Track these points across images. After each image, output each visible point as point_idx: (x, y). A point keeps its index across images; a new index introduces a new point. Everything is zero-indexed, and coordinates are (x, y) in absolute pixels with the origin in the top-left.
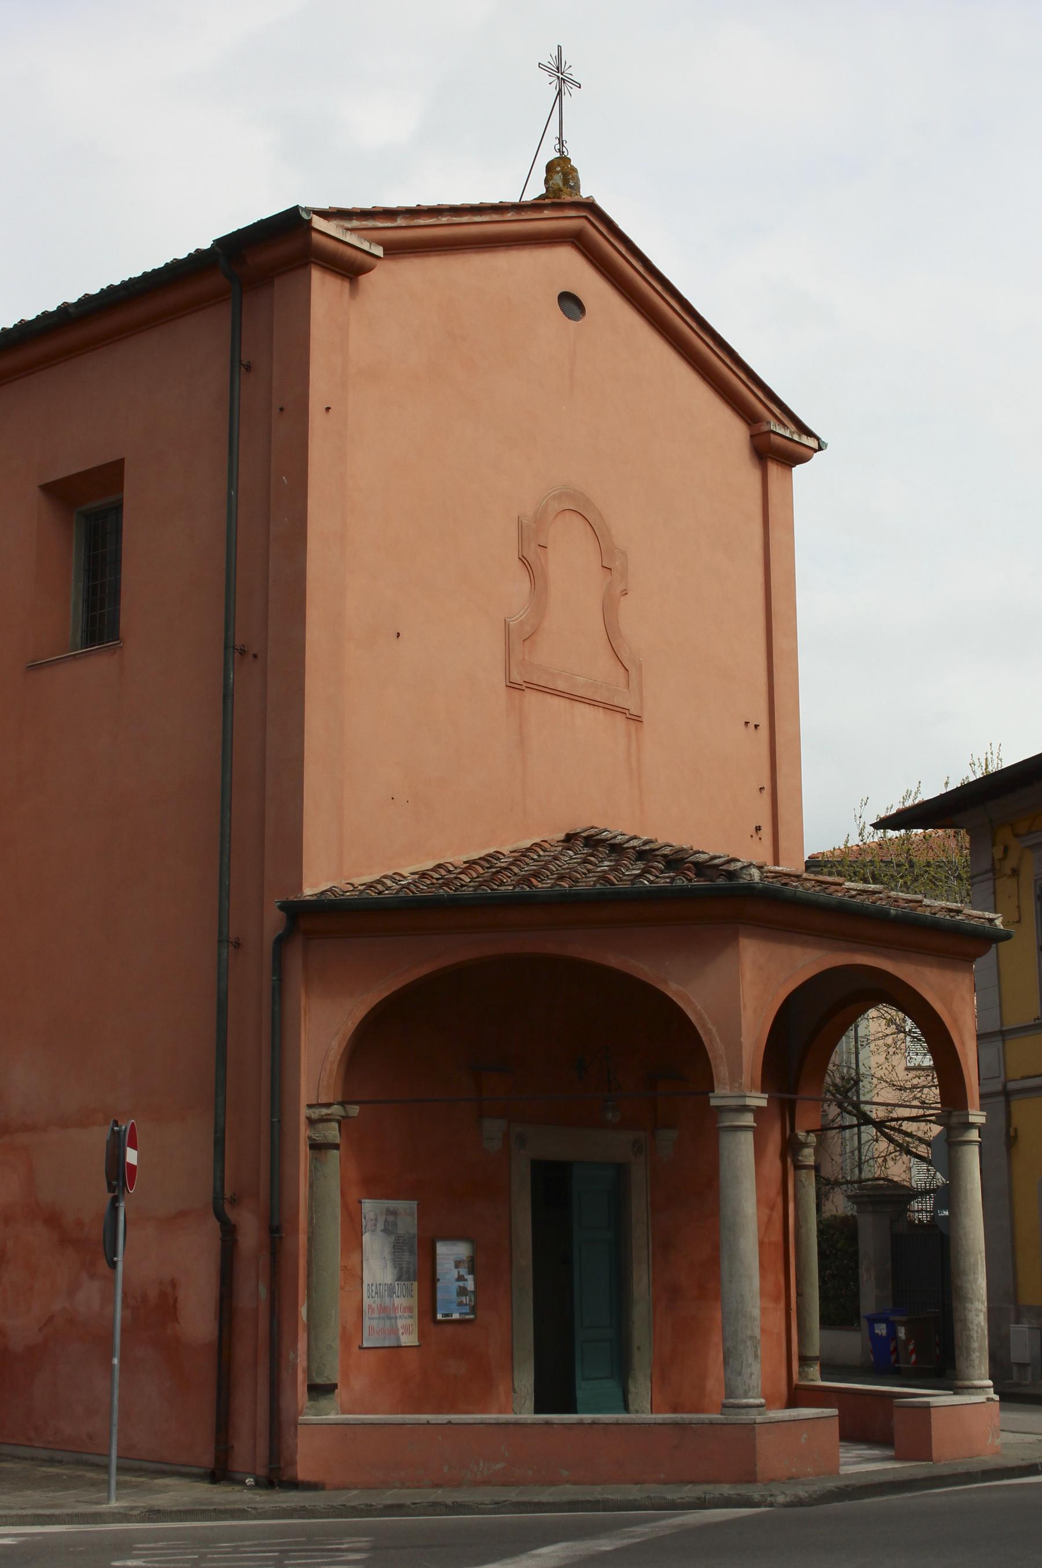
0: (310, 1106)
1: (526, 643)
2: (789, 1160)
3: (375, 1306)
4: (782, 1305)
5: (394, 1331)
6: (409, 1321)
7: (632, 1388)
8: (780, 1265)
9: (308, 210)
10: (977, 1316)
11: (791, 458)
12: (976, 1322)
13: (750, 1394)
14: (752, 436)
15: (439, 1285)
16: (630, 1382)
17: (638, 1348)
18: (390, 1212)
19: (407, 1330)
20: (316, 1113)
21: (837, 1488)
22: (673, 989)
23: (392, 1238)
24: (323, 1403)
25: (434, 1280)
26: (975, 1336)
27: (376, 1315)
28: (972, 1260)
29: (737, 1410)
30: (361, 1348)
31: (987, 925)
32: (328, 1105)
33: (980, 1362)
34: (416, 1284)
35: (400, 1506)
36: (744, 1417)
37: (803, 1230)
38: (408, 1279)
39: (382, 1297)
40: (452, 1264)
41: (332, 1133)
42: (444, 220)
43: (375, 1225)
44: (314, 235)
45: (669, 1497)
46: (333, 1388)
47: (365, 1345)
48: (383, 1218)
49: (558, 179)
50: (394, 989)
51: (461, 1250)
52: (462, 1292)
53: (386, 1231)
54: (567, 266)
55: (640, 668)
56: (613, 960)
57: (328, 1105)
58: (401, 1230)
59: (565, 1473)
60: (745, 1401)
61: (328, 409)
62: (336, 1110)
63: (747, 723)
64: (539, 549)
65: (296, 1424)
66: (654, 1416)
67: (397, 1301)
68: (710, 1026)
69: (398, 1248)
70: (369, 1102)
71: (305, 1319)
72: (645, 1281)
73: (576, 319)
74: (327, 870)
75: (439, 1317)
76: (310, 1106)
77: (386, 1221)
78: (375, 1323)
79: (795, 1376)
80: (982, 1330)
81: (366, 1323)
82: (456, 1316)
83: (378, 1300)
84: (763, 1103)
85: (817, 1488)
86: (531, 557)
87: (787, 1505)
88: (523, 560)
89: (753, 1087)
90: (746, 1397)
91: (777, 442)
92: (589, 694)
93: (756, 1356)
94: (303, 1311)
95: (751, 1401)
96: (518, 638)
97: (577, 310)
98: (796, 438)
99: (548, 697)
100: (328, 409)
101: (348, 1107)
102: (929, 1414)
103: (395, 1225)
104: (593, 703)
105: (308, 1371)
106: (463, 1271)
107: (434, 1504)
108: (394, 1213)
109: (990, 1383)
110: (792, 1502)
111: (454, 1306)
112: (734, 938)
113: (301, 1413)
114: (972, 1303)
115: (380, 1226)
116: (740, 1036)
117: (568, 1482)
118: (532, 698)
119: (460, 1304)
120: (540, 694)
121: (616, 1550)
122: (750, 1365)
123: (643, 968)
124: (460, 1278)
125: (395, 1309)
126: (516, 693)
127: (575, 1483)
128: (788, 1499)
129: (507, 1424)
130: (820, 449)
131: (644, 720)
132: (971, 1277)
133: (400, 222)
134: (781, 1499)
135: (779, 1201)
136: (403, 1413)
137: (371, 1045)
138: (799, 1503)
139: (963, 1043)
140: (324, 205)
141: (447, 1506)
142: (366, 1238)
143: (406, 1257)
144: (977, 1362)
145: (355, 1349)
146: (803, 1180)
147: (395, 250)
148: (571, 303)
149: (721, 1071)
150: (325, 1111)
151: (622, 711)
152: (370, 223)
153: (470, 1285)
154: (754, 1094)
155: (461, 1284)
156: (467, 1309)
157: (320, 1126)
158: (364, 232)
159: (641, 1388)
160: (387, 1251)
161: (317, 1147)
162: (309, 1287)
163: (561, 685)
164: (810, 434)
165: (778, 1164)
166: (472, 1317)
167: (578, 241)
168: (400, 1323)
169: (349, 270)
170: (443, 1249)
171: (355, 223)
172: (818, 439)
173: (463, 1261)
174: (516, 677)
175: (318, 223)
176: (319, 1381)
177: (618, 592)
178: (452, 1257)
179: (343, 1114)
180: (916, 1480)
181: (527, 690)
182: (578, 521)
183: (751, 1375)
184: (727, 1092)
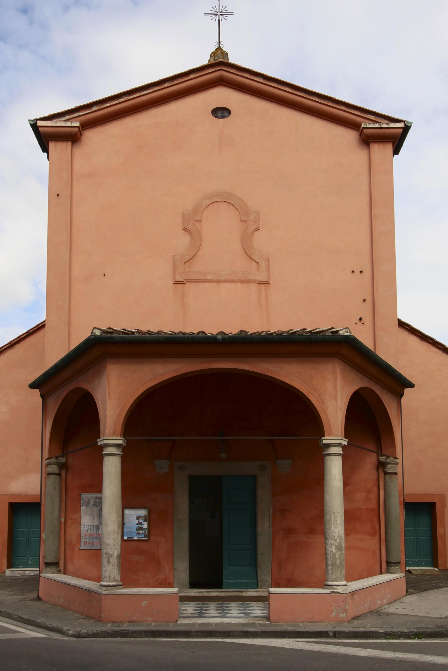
1: (187, 264)
2: (380, 471)
4: (377, 537)
7: (259, 571)
8: (376, 519)
10: (331, 547)
12: (330, 550)
13: (105, 580)
15: (125, 526)
16: (258, 568)
21: (113, 631)
26: (329, 558)
28: (328, 517)
30: (79, 549)
33: (332, 572)
37: (387, 503)
40: (135, 518)
44: (40, 129)
47: (81, 548)
51: (143, 512)
52: (141, 529)
54: (220, 96)
55: (268, 260)
64: (196, 223)
73: (225, 117)
77: (95, 501)
78: (87, 540)
81: (83, 540)
82: (136, 538)
86: (190, 227)
88: (185, 229)
89: (114, 434)
92: (230, 278)
97: (225, 113)
98: (384, 126)
99: (226, 283)
110: (74, 634)
111: (135, 534)
114: (328, 540)
119: (139, 534)
120: (197, 283)
124: (139, 523)
131: (271, 283)
134: (71, 632)
135: (375, 489)
140: (46, 114)
142: (83, 508)
144: (330, 572)
146: (387, 479)
148: (221, 112)
151: (254, 281)
152: (76, 115)
153: (145, 525)
154: (114, 438)
155: (140, 526)
163: (209, 277)
165: (375, 472)
166: (146, 539)
171: (67, 117)
172: (404, 121)
173: (142, 517)
174: (179, 279)
177: (252, 230)
178: (136, 515)
180: (191, 632)
181: (186, 283)
183: (105, 571)
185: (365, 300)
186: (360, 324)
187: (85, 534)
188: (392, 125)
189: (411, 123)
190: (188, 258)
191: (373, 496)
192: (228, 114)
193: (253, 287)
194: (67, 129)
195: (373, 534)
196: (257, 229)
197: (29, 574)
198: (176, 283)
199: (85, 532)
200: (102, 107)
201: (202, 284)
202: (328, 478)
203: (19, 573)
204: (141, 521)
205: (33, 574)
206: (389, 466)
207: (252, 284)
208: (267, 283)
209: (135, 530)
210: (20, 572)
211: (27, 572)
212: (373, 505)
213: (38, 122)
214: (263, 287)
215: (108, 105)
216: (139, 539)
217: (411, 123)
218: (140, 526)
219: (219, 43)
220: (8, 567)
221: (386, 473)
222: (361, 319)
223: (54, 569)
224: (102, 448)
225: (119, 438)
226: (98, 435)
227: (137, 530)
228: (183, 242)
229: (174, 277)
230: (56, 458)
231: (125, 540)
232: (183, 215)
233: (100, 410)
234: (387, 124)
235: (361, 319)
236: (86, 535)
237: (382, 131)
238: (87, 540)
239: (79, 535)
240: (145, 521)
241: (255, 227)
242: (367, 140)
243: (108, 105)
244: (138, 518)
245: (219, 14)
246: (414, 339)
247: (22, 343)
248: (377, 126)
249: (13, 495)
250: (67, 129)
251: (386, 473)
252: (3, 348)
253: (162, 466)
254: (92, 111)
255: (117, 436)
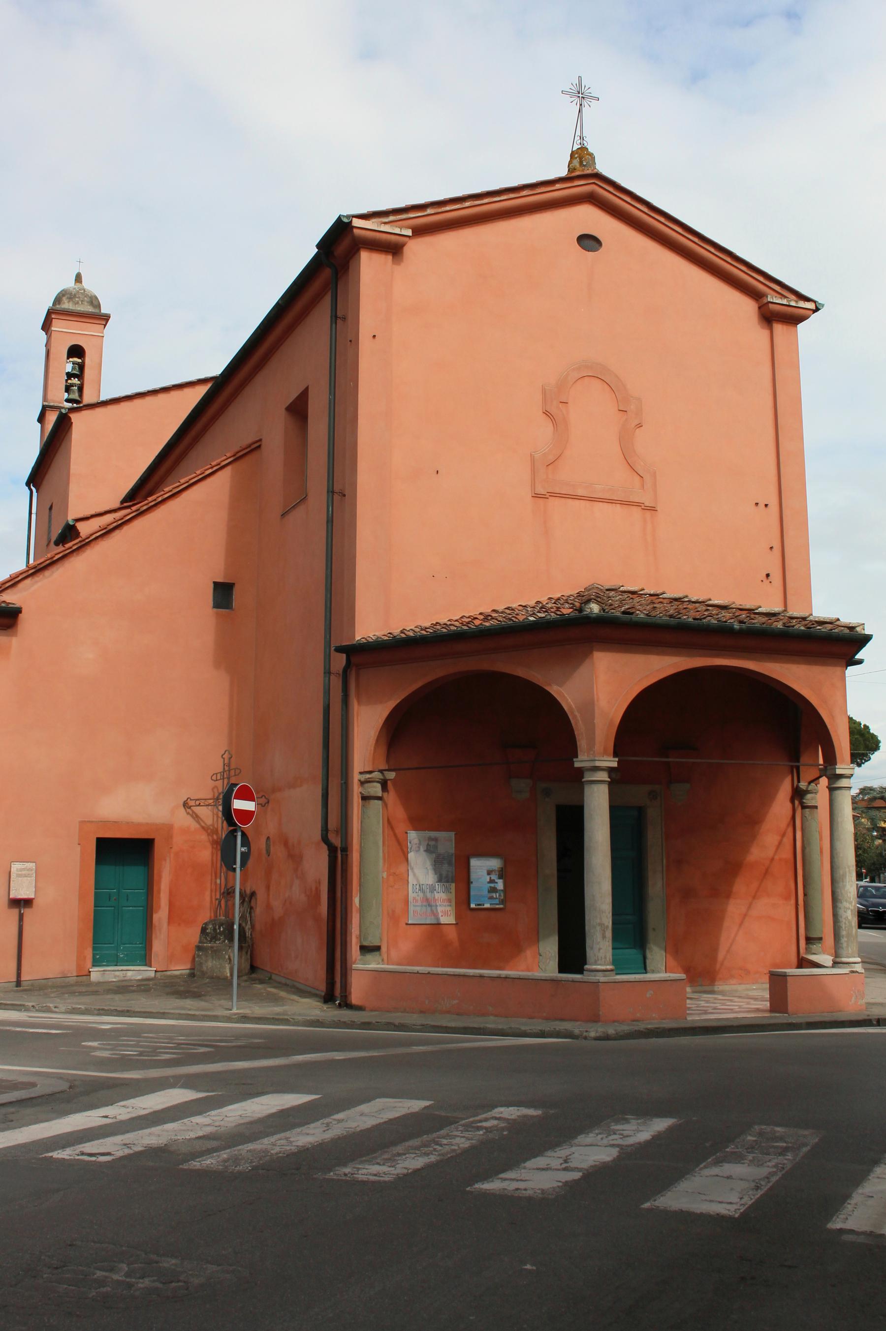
0: (361, 773)
2: (797, 802)
3: (418, 898)
4: (793, 901)
5: (435, 914)
6: (449, 908)
7: (648, 955)
8: (791, 874)
9: (348, 217)
11: (794, 319)
12: (844, 917)
13: (599, 962)
14: (759, 308)
15: (472, 885)
17: (654, 929)
18: (430, 839)
19: (446, 914)
20: (364, 777)
21: (647, 1029)
22: (554, 690)
23: (434, 855)
24: (369, 957)
25: (469, 882)
27: (419, 903)
29: (592, 974)
31: (847, 631)
32: (370, 772)
33: (848, 945)
34: (453, 885)
35: (369, 1023)
36: (592, 978)
37: (807, 850)
38: (448, 882)
39: (424, 892)
41: (376, 789)
42: (467, 204)
43: (419, 847)
44: (355, 231)
45: (523, 1028)
46: (377, 949)
47: (410, 922)
48: (426, 843)
49: (576, 163)
50: (403, 697)
51: (495, 863)
52: (493, 890)
53: (428, 850)
54: (588, 218)
55: (654, 475)
56: (521, 672)
57: (370, 772)
58: (441, 849)
59: (490, 1009)
60: (594, 967)
61: (374, 336)
62: (377, 775)
63: (757, 504)
64: (561, 405)
65: (351, 969)
66: (668, 975)
67: (437, 896)
68: (577, 713)
69: (438, 862)
70: (417, 768)
71: (358, 905)
72: (659, 884)
74: (370, 625)
75: (473, 906)
76: (361, 773)
78: (418, 909)
79: (802, 950)
80: (850, 922)
81: (411, 908)
82: (487, 906)
83: (421, 895)
84: (615, 765)
85: (625, 1028)
87: (597, 1039)
88: (546, 413)
89: (605, 752)
90: (596, 963)
91: (779, 309)
92: (607, 496)
93: (604, 937)
94: (356, 901)
95: (599, 967)
96: (546, 464)
98: (793, 304)
100: (374, 336)
101: (385, 773)
102: (786, 983)
103: (436, 847)
104: (611, 501)
105: (359, 937)
106: (494, 877)
107: (388, 1024)
108: (436, 840)
109: (859, 960)
112: (591, 652)
113: (354, 963)
115: (422, 849)
116: (594, 719)
117: (492, 1015)
118: (554, 502)
119: (491, 898)
121: (344, 1060)
122: (598, 943)
123: (535, 675)
124: (492, 881)
125: (435, 900)
126: (541, 501)
127: (496, 1016)
128: (598, 1035)
129: (459, 975)
130: (817, 310)
131: (658, 509)
132: (841, 884)
133: (429, 211)
134: (593, 1034)
135: (790, 830)
136: (442, 967)
137: (395, 731)
138: (607, 1038)
139: (832, 717)
140: (364, 211)
141: (395, 1025)
142: (411, 856)
143: (446, 867)
144: (845, 945)
145: (402, 924)
147: (420, 231)
149: (582, 743)
150: (368, 776)
151: (638, 505)
153: (500, 885)
154: (605, 758)
155: (492, 885)
156: (497, 901)
157: (366, 785)
158: (400, 223)
159: (657, 955)
160: (429, 864)
161: (365, 798)
162: (360, 885)
163: (580, 492)
164: (807, 299)
165: (789, 805)
166: (502, 906)
167: (592, 199)
168: (440, 909)
169: (393, 249)
170: (474, 862)
171: (391, 218)
172: (815, 302)
174: (540, 490)
175: (357, 222)
176: (365, 944)
177: (633, 426)
179: (382, 777)
182: (596, 383)
183: (600, 949)
184: (585, 758)
185: (771, 548)
186: (766, 582)
187: (414, 898)
188: (802, 304)
189: (823, 305)
190: (551, 458)
191: (788, 840)
192: (597, 245)
193: (636, 512)
194: (393, 237)
195: (787, 898)
196: (640, 426)
197: (133, 978)
198: (537, 496)
199: (415, 895)
200: (440, 210)
201: (570, 501)
202: (839, 820)
203: (115, 976)
204: (494, 877)
205: (139, 977)
206: (809, 796)
207: (635, 509)
208: (653, 509)
209: (485, 892)
210: (117, 973)
211: (129, 974)
212: (786, 853)
213: (354, 220)
214: (648, 514)
215: (448, 208)
216: (493, 906)
217: (823, 305)
218: (492, 885)
219: (582, 138)
220: (96, 963)
221: (804, 807)
222: (768, 575)
223: (246, 966)
224: (580, 772)
225: (612, 759)
226: (573, 751)
227: (489, 892)
228: (544, 431)
229: (533, 485)
230: (381, 771)
231: (473, 909)
232: (544, 392)
233: (575, 717)
234: (796, 302)
235: (768, 575)
236: (417, 901)
237: (789, 309)
238: (418, 909)
239: (407, 902)
240: (499, 878)
241: (637, 422)
242: (770, 318)
243: (448, 208)
244: (489, 873)
245: (581, 95)
246: (149, 400)
247: (126, 528)
248: (785, 302)
249: (105, 823)
250: (393, 237)
251: (804, 807)
252: (94, 537)
253: (521, 787)
254: (425, 213)
255: (608, 755)
